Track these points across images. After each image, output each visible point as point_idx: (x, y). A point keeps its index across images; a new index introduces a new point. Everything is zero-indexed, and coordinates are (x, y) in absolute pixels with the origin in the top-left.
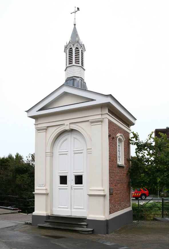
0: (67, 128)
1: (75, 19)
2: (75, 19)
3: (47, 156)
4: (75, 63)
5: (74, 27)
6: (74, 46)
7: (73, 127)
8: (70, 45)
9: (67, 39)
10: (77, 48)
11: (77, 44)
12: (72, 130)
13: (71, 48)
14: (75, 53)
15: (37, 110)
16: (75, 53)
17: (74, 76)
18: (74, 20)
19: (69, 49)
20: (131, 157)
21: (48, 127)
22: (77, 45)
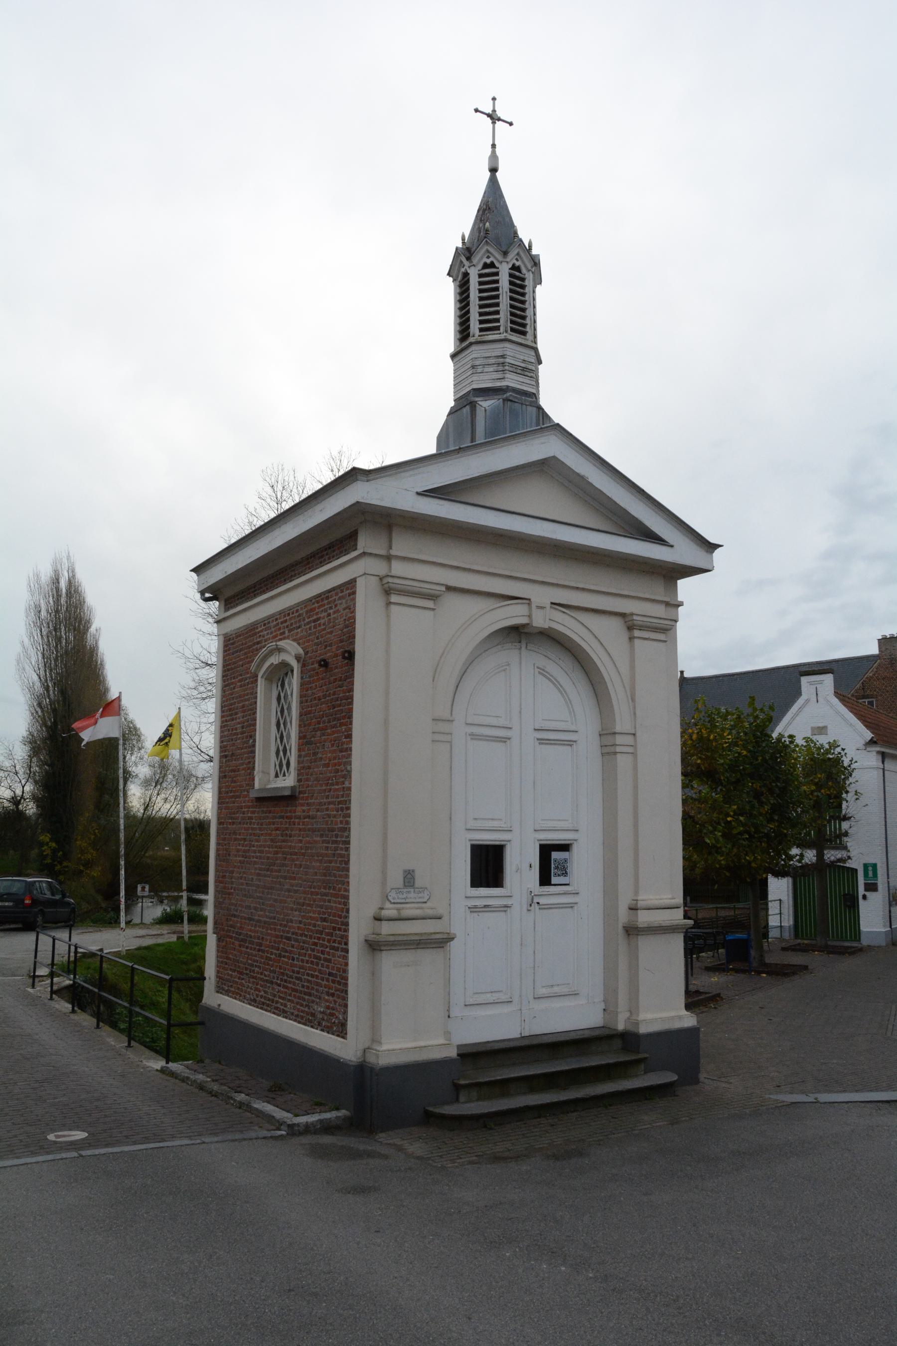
0: (540, 621)
1: (494, 146)
2: (494, 146)
3: (630, 750)
4: (512, 330)
5: (491, 176)
6: (508, 260)
7: (566, 625)
8: (488, 251)
9: (461, 223)
10: (518, 269)
11: (516, 252)
12: (552, 639)
13: (492, 265)
14: (495, 282)
15: (420, 490)
16: (495, 282)
17: (474, 390)
18: (489, 153)
19: (480, 266)
20: (127, 817)
21: (449, 589)
22: (518, 254)
